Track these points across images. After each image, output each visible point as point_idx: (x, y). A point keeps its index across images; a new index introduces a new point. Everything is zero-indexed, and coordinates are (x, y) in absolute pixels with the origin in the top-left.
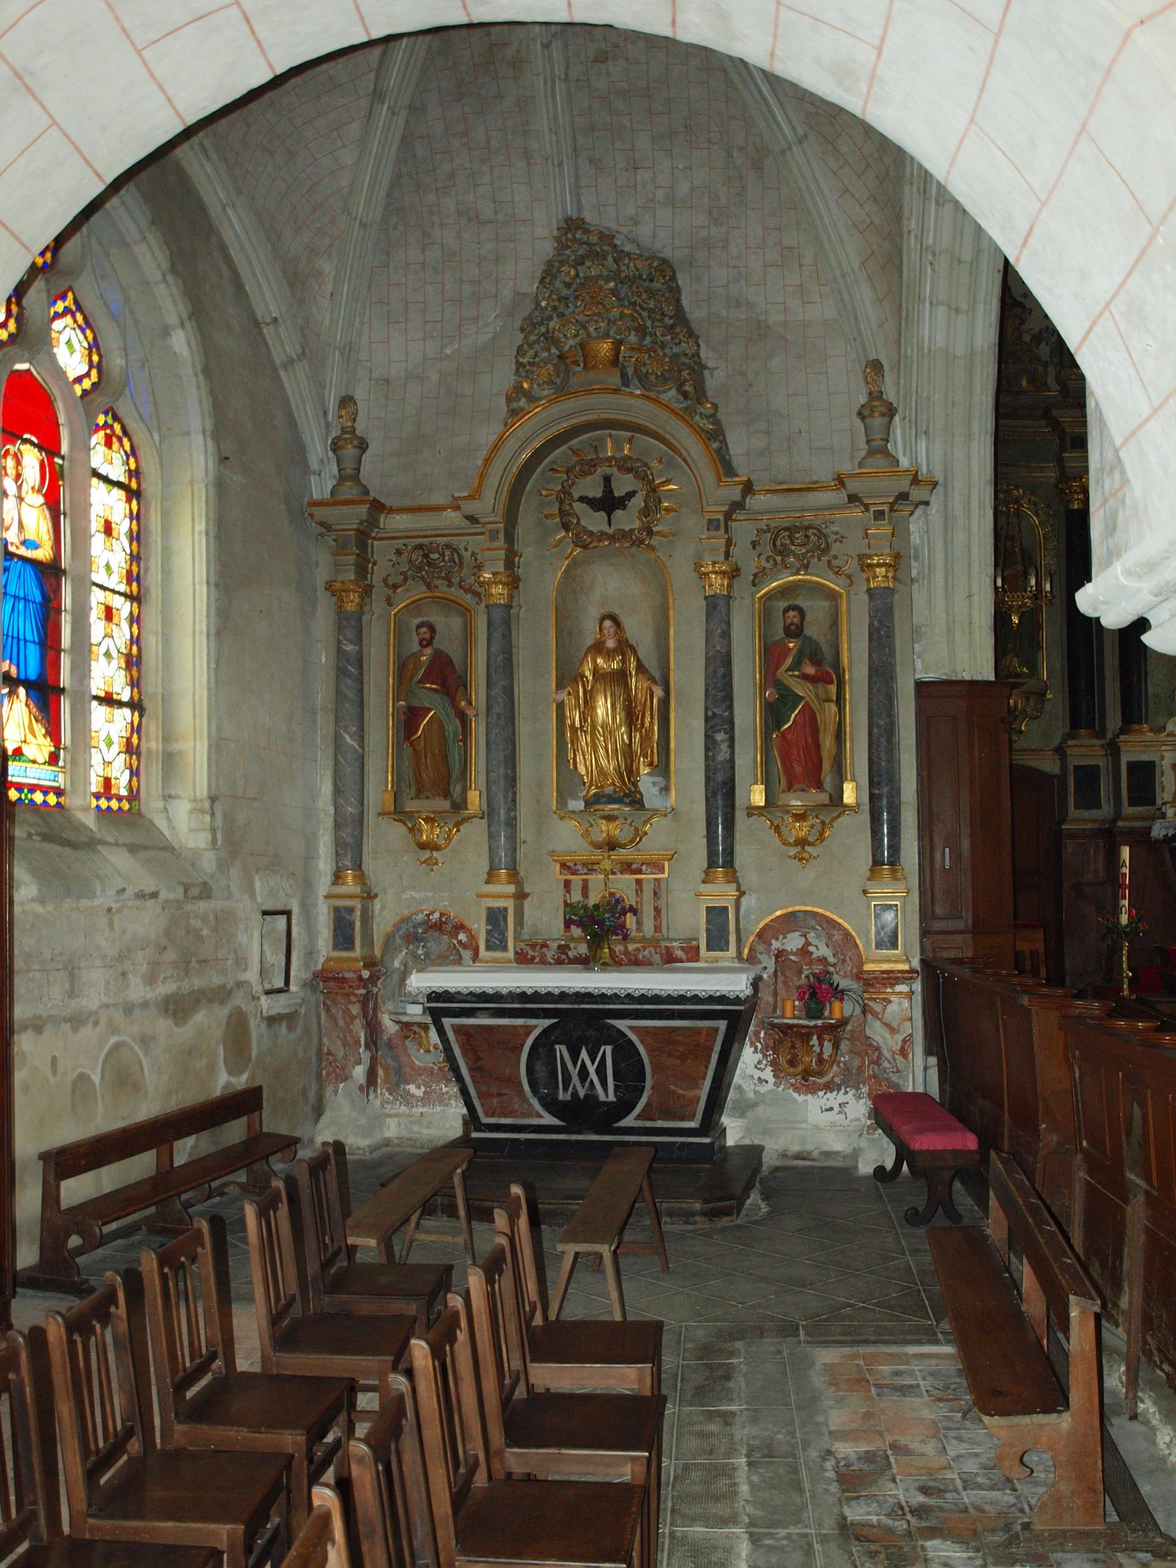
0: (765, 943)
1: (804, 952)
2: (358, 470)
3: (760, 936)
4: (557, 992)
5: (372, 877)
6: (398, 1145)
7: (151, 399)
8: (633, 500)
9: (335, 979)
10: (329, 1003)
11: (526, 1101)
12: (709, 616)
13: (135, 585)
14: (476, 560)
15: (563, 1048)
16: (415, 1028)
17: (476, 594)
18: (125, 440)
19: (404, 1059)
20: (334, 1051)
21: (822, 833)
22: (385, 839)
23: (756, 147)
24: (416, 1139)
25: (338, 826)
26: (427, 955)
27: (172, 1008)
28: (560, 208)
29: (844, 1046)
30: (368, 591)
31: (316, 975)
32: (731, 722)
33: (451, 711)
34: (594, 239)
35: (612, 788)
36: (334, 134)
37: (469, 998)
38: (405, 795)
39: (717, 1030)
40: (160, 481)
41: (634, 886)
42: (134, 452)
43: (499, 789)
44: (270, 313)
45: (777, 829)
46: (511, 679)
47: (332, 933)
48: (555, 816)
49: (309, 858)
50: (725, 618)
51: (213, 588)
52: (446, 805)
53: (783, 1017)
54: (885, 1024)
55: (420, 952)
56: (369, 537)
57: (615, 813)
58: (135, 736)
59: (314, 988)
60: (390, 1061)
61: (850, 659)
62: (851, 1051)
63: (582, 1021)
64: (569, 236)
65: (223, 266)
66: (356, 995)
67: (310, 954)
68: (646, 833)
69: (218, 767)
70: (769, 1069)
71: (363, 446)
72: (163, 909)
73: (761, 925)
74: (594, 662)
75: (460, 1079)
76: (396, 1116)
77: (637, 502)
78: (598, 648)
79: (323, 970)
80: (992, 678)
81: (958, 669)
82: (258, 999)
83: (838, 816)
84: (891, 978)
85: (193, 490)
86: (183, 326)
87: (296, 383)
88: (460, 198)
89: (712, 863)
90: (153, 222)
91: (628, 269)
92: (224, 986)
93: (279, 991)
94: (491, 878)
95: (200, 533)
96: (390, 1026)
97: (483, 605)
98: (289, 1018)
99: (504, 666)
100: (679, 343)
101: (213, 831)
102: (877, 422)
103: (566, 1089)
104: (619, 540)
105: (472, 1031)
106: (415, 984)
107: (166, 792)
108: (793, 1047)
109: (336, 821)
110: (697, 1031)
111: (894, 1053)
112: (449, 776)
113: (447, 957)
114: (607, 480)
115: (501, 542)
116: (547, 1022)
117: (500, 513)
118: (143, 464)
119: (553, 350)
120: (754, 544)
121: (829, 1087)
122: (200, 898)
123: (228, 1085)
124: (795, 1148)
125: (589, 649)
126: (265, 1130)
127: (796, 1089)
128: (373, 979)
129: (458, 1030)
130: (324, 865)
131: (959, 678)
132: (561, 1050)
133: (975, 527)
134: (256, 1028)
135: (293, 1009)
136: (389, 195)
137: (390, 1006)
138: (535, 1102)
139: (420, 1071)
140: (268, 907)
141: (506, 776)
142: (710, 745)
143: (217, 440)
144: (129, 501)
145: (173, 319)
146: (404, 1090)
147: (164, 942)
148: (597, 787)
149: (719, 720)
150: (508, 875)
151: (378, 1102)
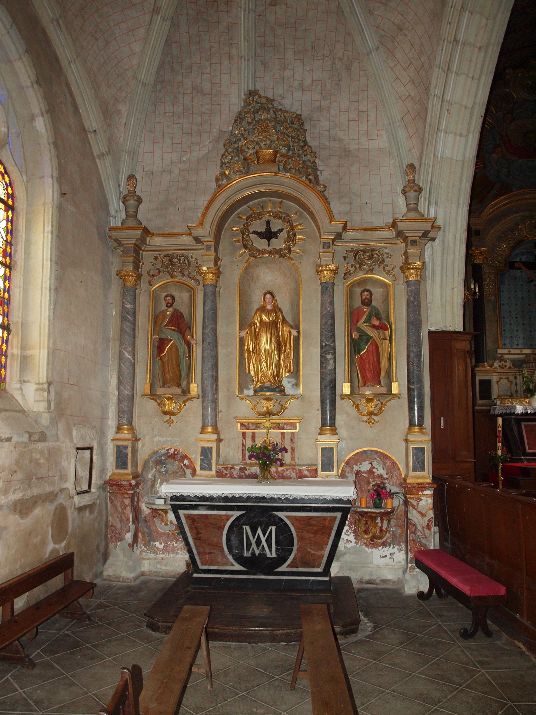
0: (350, 467)
1: (370, 472)
2: (137, 213)
3: (347, 463)
4: (245, 496)
5: (138, 429)
6: (149, 575)
7: (22, 156)
8: (281, 233)
9: (116, 485)
10: (113, 498)
11: (225, 557)
12: (322, 294)
13: (8, 258)
14: (197, 263)
15: (248, 528)
16: (160, 512)
17: (198, 281)
18: (6, 176)
19: (153, 528)
20: (115, 525)
21: (381, 409)
22: (145, 409)
23: (348, 58)
24: (159, 572)
25: (120, 401)
26: (166, 472)
27: (18, 508)
28: (246, 85)
29: (393, 522)
30: (139, 277)
31: (106, 483)
32: (334, 349)
33: (182, 341)
34: (264, 101)
35: (269, 383)
36: (131, 33)
37: (194, 499)
38: (156, 386)
39: (335, 518)
40: (26, 202)
41: (280, 436)
42: (11, 184)
43: (208, 383)
44: (92, 127)
45: (357, 407)
46: (216, 324)
47: (115, 460)
48: (238, 398)
49: (104, 418)
50: (332, 294)
51: (54, 264)
52: (179, 391)
53: (360, 507)
54: (418, 512)
55: (163, 470)
56: (141, 249)
57: (272, 396)
58: (4, 345)
59: (104, 489)
60: (145, 529)
61: (395, 317)
62: (396, 525)
63: (259, 513)
64: (251, 98)
65: (68, 95)
66: (128, 494)
67: (103, 470)
68: (286, 408)
69: (53, 365)
70: (352, 534)
71: (139, 201)
72: (15, 447)
73: (348, 458)
74: (261, 316)
75: (187, 544)
76: (149, 559)
77: (284, 235)
78: (262, 309)
79: (110, 480)
80: (461, 330)
81: (448, 325)
82: (73, 498)
83: (390, 400)
84: (421, 487)
85: (44, 208)
86: (42, 115)
87: (105, 167)
88: (193, 80)
89: (324, 424)
90: (27, 51)
91: (281, 116)
92: (53, 492)
93: (85, 492)
94: (203, 430)
95: (48, 232)
96: (145, 510)
97: (201, 285)
98: (90, 507)
99: (212, 317)
100: (307, 155)
101: (49, 402)
102: (412, 195)
103: (248, 550)
104: (272, 254)
105: (196, 518)
106: (164, 491)
107: (22, 379)
108: (366, 523)
109: (119, 398)
110: (325, 518)
111: (423, 527)
112: (180, 376)
113: (177, 473)
114: (268, 223)
115: (212, 251)
116: (239, 513)
117: (213, 235)
118: (16, 192)
119: (241, 156)
120: (345, 258)
121: (384, 545)
122: (39, 441)
123: (54, 550)
124: (367, 578)
125: (258, 310)
126: (75, 579)
127: (367, 546)
128: (137, 485)
129: (187, 517)
130: (112, 422)
131: (448, 330)
132: (246, 528)
133: (457, 253)
134: (71, 514)
135: (93, 502)
136: (157, 72)
137: (146, 499)
138: (230, 558)
139: (162, 535)
140: (80, 445)
141: (213, 375)
142: (323, 361)
143: (60, 183)
144: (6, 210)
145: (37, 111)
146: (153, 545)
147: (15, 468)
148: (261, 383)
149: (327, 349)
150: (213, 429)
151: (138, 551)
